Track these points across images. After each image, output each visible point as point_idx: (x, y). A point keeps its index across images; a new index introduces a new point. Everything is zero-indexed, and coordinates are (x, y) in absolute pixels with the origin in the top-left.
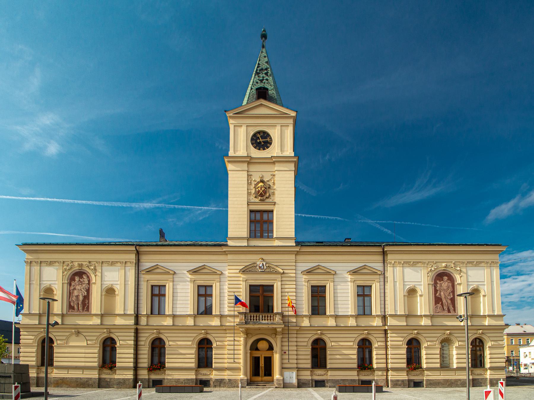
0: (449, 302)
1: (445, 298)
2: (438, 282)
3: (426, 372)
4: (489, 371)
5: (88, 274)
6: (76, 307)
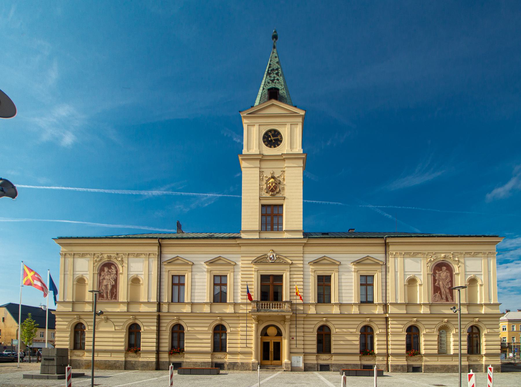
0: (447, 291)
2: (437, 272)
3: (424, 358)
4: (484, 357)
5: (116, 265)
6: (105, 296)
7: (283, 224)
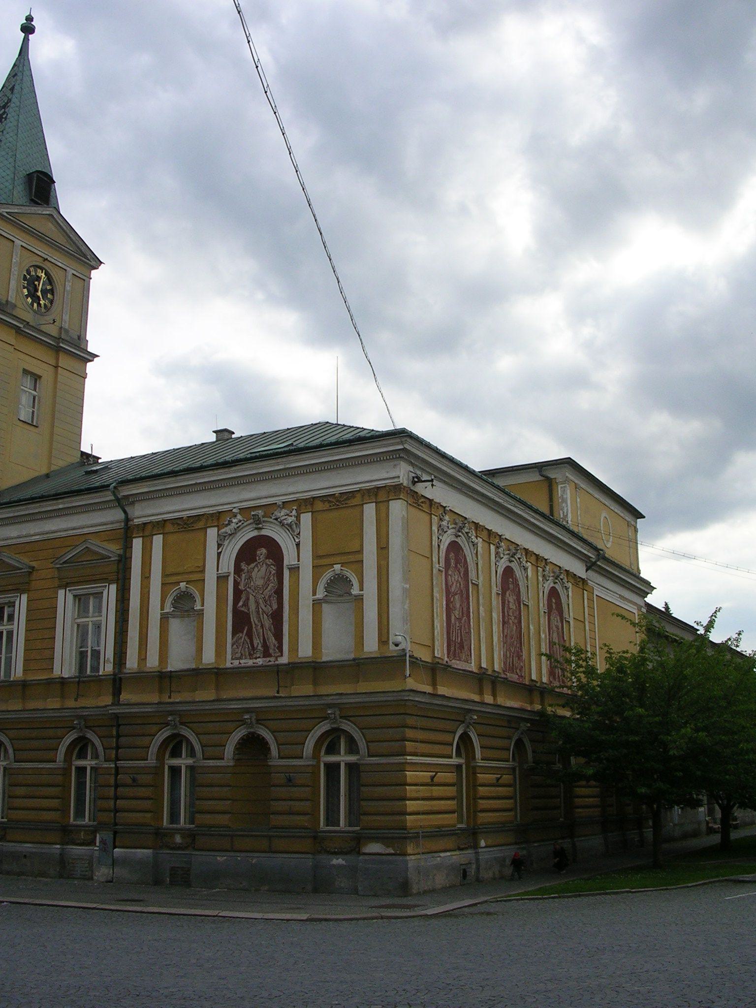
0: (267, 622)
1: (258, 612)
2: (243, 566)
7: (129, 599)
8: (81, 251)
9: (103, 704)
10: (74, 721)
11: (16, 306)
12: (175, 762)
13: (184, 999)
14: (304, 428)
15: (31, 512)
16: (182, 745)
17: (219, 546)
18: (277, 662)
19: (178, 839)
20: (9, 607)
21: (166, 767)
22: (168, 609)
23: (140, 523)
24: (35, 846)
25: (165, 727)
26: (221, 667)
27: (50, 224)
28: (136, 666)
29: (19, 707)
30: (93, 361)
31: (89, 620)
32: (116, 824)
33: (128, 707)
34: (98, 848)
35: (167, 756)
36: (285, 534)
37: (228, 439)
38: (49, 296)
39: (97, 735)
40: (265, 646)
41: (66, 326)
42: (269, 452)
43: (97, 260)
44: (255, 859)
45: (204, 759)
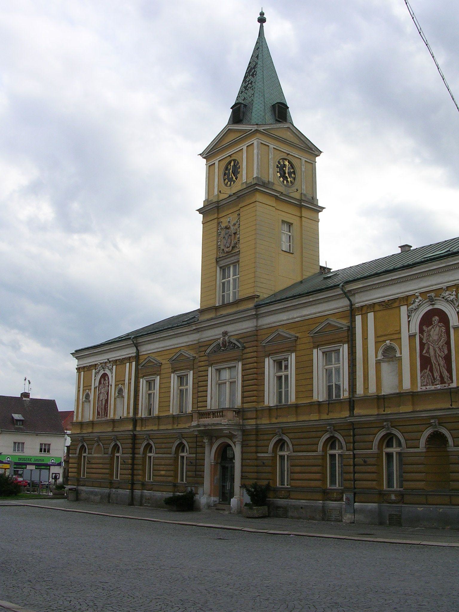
0: (442, 362)
1: (436, 356)
2: (425, 328)
8: (308, 146)
9: (344, 416)
10: (326, 427)
11: (274, 184)
12: (389, 450)
13: (405, 594)
14: (379, 260)
15: (294, 304)
16: (393, 440)
17: (409, 316)
18: (449, 387)
19: (393, 497)
20: (285, 361)
21: (384, 454)
22: (380, 357)
23: (360, 306)
24: (307, 501)
25: (383, 429)
26: (415, 391)
27: (289, 133)
28: (362, 392)
29: (294, 420)
30: (322, 211)
31: (333, 366)
32: (355, 488)
33: (359, 417)
34: (344, 503)
35: (384, 447)
36: (448, 306)
37: (408, 251)
38: (293, 175)
39: (341, 435)
40: (441, 377)
41: (305, 192)
42: (435, 256)
43: (318, 150)
44: (441, 509)
45: (407, 448)
